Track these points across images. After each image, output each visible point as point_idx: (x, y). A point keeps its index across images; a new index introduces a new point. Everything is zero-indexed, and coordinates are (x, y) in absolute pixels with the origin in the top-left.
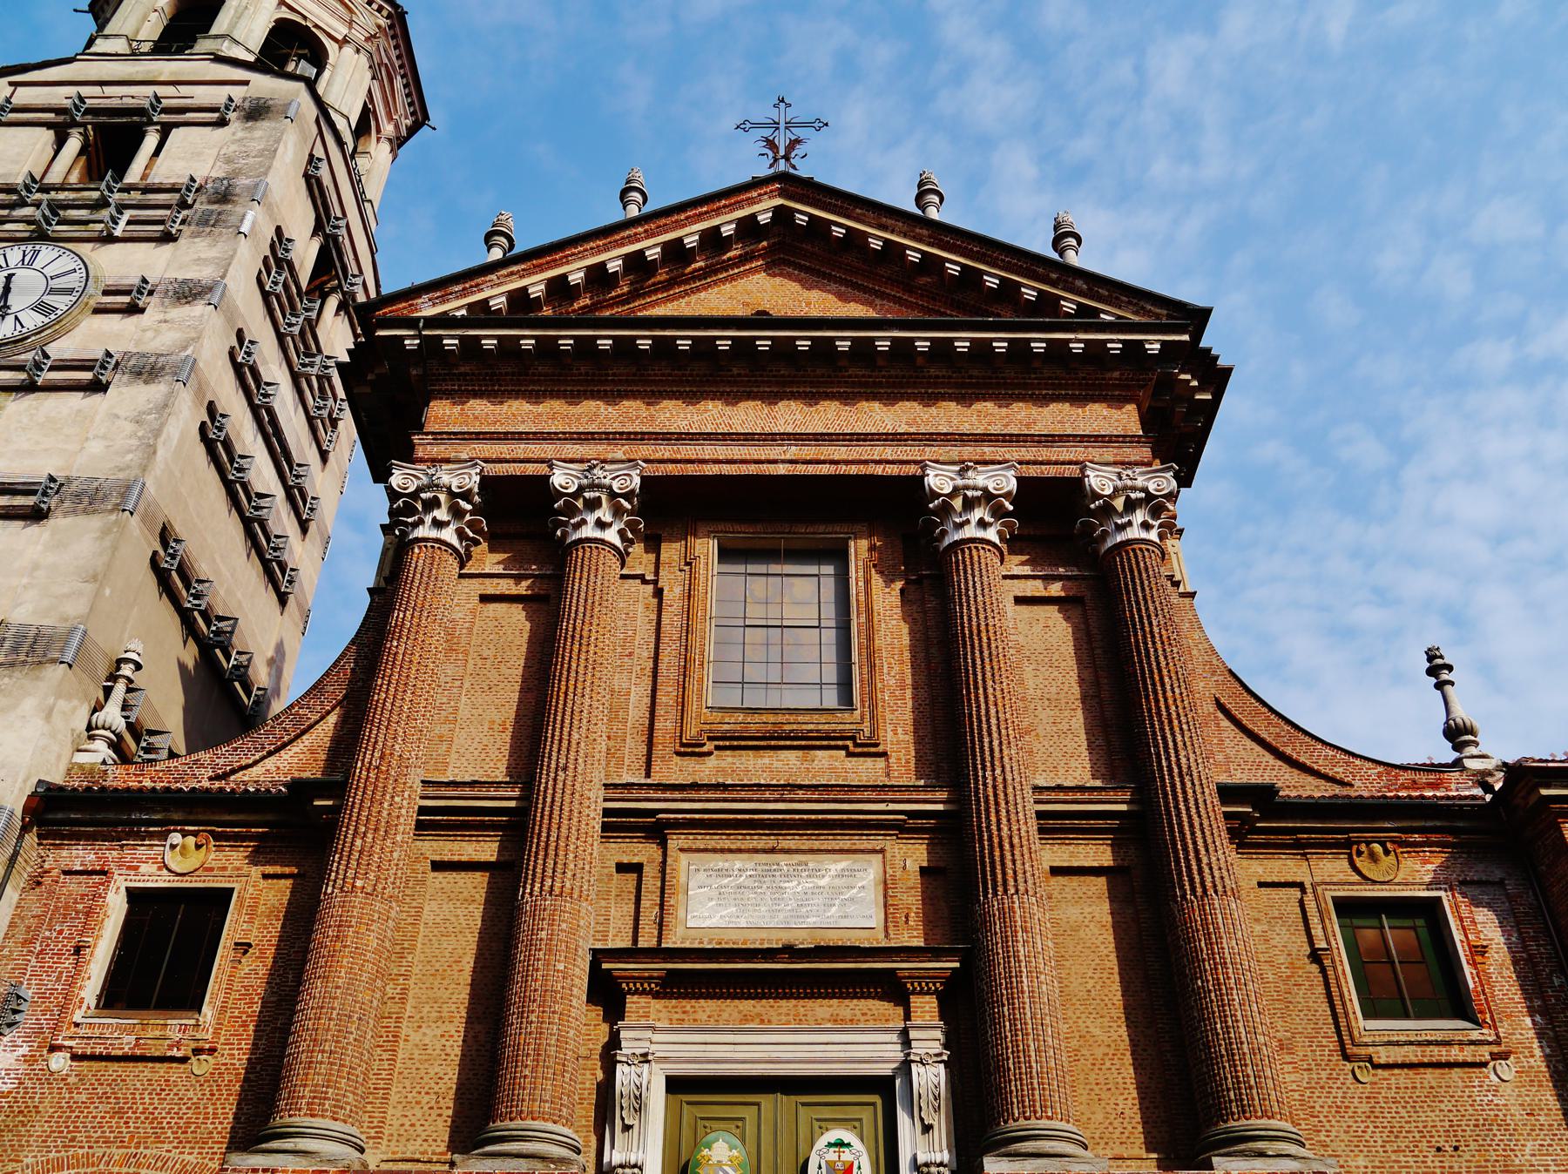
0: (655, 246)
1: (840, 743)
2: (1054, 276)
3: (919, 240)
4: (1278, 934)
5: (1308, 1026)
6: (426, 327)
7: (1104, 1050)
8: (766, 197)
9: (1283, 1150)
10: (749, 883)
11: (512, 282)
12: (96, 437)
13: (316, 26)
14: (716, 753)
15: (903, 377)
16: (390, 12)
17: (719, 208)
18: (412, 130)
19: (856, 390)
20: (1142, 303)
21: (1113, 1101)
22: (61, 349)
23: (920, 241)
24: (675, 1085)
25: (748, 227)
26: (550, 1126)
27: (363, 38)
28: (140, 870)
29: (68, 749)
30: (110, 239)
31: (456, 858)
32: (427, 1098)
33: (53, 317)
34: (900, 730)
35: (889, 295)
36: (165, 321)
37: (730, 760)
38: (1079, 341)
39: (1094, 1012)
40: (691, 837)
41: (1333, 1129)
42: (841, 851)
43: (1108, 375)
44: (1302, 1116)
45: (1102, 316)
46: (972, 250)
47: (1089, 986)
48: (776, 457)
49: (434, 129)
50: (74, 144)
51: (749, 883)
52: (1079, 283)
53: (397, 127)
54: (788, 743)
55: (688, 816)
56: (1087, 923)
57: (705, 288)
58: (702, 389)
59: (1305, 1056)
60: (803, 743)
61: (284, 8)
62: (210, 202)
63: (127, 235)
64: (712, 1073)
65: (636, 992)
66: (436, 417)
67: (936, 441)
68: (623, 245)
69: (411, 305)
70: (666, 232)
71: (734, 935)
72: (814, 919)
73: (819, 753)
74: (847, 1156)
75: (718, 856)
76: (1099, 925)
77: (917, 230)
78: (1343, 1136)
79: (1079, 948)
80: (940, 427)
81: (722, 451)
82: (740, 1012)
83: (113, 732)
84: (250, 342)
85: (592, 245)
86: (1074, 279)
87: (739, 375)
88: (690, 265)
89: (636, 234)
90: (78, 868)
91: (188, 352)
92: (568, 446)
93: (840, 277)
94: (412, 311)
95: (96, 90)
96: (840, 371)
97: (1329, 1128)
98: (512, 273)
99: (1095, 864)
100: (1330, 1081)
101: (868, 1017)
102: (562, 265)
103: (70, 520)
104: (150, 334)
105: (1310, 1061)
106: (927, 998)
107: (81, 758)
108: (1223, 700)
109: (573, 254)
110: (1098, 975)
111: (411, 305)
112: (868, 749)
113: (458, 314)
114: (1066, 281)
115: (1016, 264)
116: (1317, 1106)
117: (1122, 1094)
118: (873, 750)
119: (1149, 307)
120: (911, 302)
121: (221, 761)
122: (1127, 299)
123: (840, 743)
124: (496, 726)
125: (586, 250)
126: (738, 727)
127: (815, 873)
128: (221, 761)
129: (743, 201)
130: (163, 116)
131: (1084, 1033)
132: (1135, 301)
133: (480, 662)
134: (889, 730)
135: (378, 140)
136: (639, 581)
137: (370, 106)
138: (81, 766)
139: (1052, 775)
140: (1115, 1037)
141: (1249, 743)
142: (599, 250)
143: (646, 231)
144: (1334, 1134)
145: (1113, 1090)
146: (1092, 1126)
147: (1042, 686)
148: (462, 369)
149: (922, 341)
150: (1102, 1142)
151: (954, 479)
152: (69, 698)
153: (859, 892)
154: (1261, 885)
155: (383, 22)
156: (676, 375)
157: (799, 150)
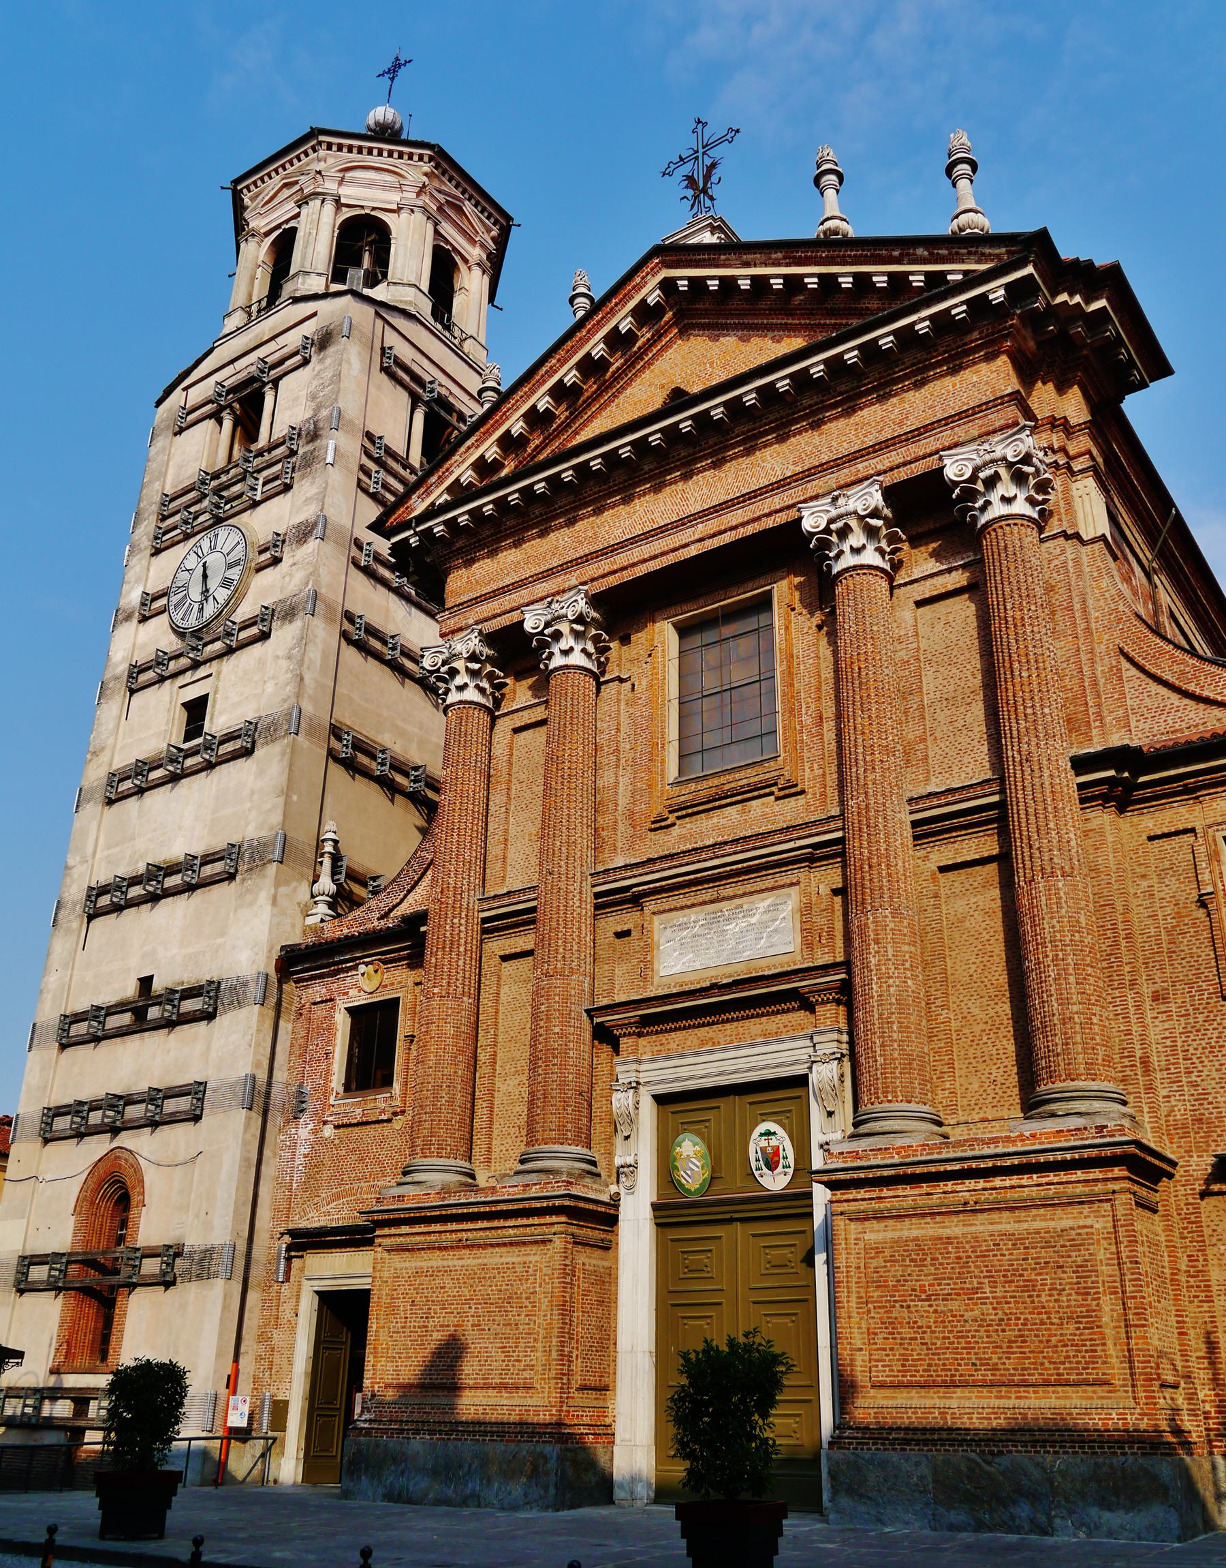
0: (570, 370)
1: (767, 790)
2: (896, 253)
3: (776, 264)
5: (1190, 973)
8: (649, 277)
9: (1072, 1109)
10: (702, 931)
11: (471, 455)
12: (269, 678)
13: (374, 209)
14: (678, 822)
15: (782, 417)
17: (612, 309)
18: (502, 241)
20: (980, 249)
21: (988, 1071)
22: (245, 611)
23: (779, 265)
24: (660, 1099)
25: (644, 313)
26: (557, 1147)
27: (414, 195)
28: (350, 994)
29: (299, 918)
30: (255, 504)
31: (513, 951)
36: (294, 564)
37: (688, 826)
39: (975, 994)
40: (659, 901)
41: (1205, 1069)
42: (768, 890)
43: (968, 339)
44: (1173, 1061)
45: (950, 277)
47: (971, 971)
48: (687, 541)
49: (519, 225)
50: (228, 423)
51: (702, 931)
52: (920, 251)
53: (483, 246)
54: (728, 801)
55: (651, 886)
56: (971, 913)
59: (1183, 1002)
60: (739, 798)
61: (344, 209)
63: (265, 496)
64: (691, 1088)
65: (823, 1002)
68: (545, 382)
69: (407, 508)
71: (692, 977)
72: (748, 953)
73: (754, 803)
74: (774, 1142)
75: (679, 913)
76: (982, 913)
77: (773, 256)
78: (1215, 1074)
79: (964, 937)
80: (823, 456)
81: (646, 550)
83: (328, 895)
84: (368, 544)
85: (520, 393)
86: (915, 249)
87: (651, 470)
88: (608, 370)
90: (319, 1000)
91: (310, 586)
93: (734, 323)
94: (410, 513)
95: (229, 370)
96: (728, 434)
97: (1201, 1069)
98: (469, 448)
99: (977, 857)
100: (1206, 1024)
103: (265, 748)
104: (287, 579)
105: (1189, 1007)
106: (829, 1006)
107: (310, 921)
108: (1126, 649)
111: (407, 508)
112: (791, 791)
113: (441, 501)
114: (908, 254)
115: (861, 256)
116: (1191, 1049)
117: (996, 1064)
118: (793, 790)
119: (987, 251)
120: (796, 324)
121: (382, 905)
122: (966, 251)
123: (767, 790)
125: (517, 401)
127: (749, 913)
128: (382, 905)
130: (272, 372)
131: (965, 1014)
132: (974, 249)
133: (518, 786)
134: (807, 768)
135: (469, 268)
136: (616, 683)
137: (448, 247)
138: (309, 926)
139: (947, 775)
140: (992, 1013)
141: (1154, 688)
142: (528, 396)
143: (559, 360)
144: (1206, 1073)
145: (989, 1062)
147: (941, 687)
148: (458, 545)
149: (849, 351)
151: (828, 511)
153: (781, 923)
155: (427, 168)
156: (605, 490)
157: (717, 174)
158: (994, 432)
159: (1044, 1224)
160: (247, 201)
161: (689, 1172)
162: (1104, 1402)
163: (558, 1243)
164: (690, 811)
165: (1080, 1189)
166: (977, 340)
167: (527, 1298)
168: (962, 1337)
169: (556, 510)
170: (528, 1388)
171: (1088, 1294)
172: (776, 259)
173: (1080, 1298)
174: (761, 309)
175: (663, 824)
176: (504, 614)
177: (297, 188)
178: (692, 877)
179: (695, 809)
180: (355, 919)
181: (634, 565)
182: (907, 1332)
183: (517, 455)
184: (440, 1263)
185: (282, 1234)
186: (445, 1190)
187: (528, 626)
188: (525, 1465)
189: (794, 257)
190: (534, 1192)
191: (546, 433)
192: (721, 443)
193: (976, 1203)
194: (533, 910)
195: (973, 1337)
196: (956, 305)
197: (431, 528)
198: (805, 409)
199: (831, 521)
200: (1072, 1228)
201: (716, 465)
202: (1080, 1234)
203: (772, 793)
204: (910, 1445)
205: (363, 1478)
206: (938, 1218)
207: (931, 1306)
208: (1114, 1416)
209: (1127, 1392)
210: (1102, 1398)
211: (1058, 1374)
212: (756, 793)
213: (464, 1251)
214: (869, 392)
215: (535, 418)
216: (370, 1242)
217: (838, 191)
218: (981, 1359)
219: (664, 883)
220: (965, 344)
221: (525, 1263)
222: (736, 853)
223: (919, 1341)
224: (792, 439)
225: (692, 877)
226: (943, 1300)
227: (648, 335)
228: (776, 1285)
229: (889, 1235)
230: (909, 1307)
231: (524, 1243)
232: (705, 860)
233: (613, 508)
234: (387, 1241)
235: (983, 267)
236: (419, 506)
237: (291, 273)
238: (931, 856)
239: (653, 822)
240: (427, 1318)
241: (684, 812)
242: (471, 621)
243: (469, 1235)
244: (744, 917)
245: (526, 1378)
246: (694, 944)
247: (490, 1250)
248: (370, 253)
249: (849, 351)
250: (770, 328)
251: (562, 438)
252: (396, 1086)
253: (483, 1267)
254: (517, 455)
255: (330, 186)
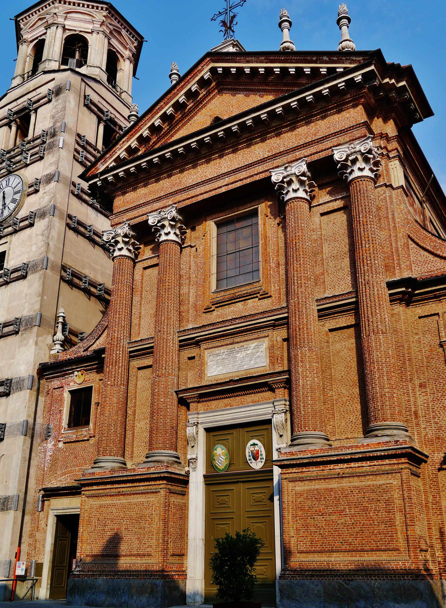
0: (169, 108)
1: (255, 296)
2: (314, 59)
3: (262, 62)
4: (426, 338)
5: (435, 375)
6: (101, 176)
7: (347, 398)
8: (205, 66)
11: (125, 145)
13: (80, 31)
14: (216, 309)
15: (263, 131)
16: (106, 8)
17: (188, 80)
19: (248, 143)
20: (351, 58)
22: (22, 214)
24: (207, 430)
25: (202, 83)
27: (99, 26)
28: (71, 385)
29: (47, 351)
30: (27, 165)
31: (143, 365)
32: (143, 444)
33: (17, 203)
34: (276, 285)
35: (261, 89)
36: (45, 193)
37: (221, 311)
38: (326, 89)
41: (441, 416)
42: (255, 339)
43: (345, 98)
45: (338, 70)
46: (281, 59)
47: (342, 374)
48: (221, 185)
50: (14, 128)
52: (325, 58)
53: (130, 50)
54: (238, 300)
57: (195, 114)
58: (195, 164)
60: (243, 299)
61: (67, 31)
62: (51, 138)
63: (31, 162)
66: (116, 206)
67: (277, 157)
68: (158, 113)
69: (96, 168)
70: (172, 100)
71: (222, 377)
73: (249, 301)
74: (257, 448)
75: (216, 349)
76: (347, 349)
77: (260, 58)
79: (340, 360)
80: (281, 149)
81: (203, 189)
82: (224, 404)
83: (60, 341)
84: (78, 184)
85: (147, 118)
86: (322, 57)
87: (205, 153)
88: (186, 108)
89: (161, 106)
90: (56, 387)
91: (52, 203)
92: (155, 205)
94: (97, 171)
95: (14, 104)
97: (439, 416)
98: (124, 142)
99: (345, 325)
101: (264, 399)
102: (139, 131)
104: (42, 199)
106: (281, 390)
107: (53, 352)
108: (411, 235)
109: (142, 125)
110: (346, 369)
111: (96, 168)
112: (265, 296)
113: (111, 165)
114: (320, 59)
115: (299, 59)
118: (266, 296)
119: (354, 58)
120: (270, 89)
121: (85, 345)
123: (255, 296)
124: (152, 316)
125: (146, 121)
126: (222, 298)
128: (85, 345)
129: (196, 72)
130: (34, 105)
131: (340, 393)
132: (348, 58)
133: (146, 293)
135: (124, 60)
136: (189, 248)
138: (52, 355)
140: (351, 392)
143: (164, 103)
146: (341, 427)
148: (119, 185)
149: (293, 102)
150: (344, 433)
151: (283, 173)
152: (42, 335)
153: (260, 353)
154: (420, 318)
155: (105, 13)
156: (185, 162)
158: (356, 139)
159: (372, 483)
160: (22, 26)
161: (220, 461)
162: (396, 558)
163: (163, 492)
164: (221, 304)
165: (387, 468)
166: (349, 98)
167: (149, 517)
168: (337, 531)
169: (163, 170)
170: (149, 555)
171: (390, 512)
172: (261, 60)
173: (387, 514)
174: (254, 82)
175: (209, 310)
176: (139, 216)
177: (45, 20)
178: (222, 333)
179: (223, 304)
180: (73, 351)
181: (197, 196)
182: (313, 529)
183: (145, 146)
184: (111, 502)
185: (40, 490)
186: (113, 470)
187: (274, 179)
188: (148, 588)
189: (270, 59)
190: (152, 470)
191: (159, 136)
192: (236, 142)
193: (343, 474)
194: (152, 347)
195: (341, 531)
196: (340, 82)
197: (107, 178)
198: (273, 127)
199: (284, 177)
200: (384, 484)
201: (234, 152)
202: (387, 487)
203: (257, 297)
204: (314, 577)
205: (76, 596)
206: (327, 480)
207: (323, 518)
208: (400, 563)
209: (406, 553)
210: (396, 556)
211: (377, 546)
212: (250, 297)
213: (121, 497)
214: (301, 120)
215: (153, 129)
216: (79, 493)
217: (289, 30)
218: (344, 540)
219: (209, 336)
220: (344, 100)
221: (148, 501)
222: (241, 323)
223: (318, 533)
224: (268, 141)
225: (222, 333)
226: (329, 515)
227: (204, 93)
228: (257, 510)
229: (306, 488)
230: (314, 518)
231: (148, 493)
232: (228, 326)
233: (188, 170)
234: (87, 493)
235: (352, 66)
236: (101, 167)
237: (43, 60)
238: (326, 324)
239: (205, 309)
240: (105, 526)
241: (219, 305)
242: (125, 220)
243: (123, 489)
244: (244, 351)
245: (148, 551)
246: (223, 362)
247: (133, 496)
248: (79, 52)
249: (293, 102)
250: (259, 91)
251: (166, 138)
252: (91, 425)
253: (130, 504)
254: (145, 146)
255: (60, 20)
